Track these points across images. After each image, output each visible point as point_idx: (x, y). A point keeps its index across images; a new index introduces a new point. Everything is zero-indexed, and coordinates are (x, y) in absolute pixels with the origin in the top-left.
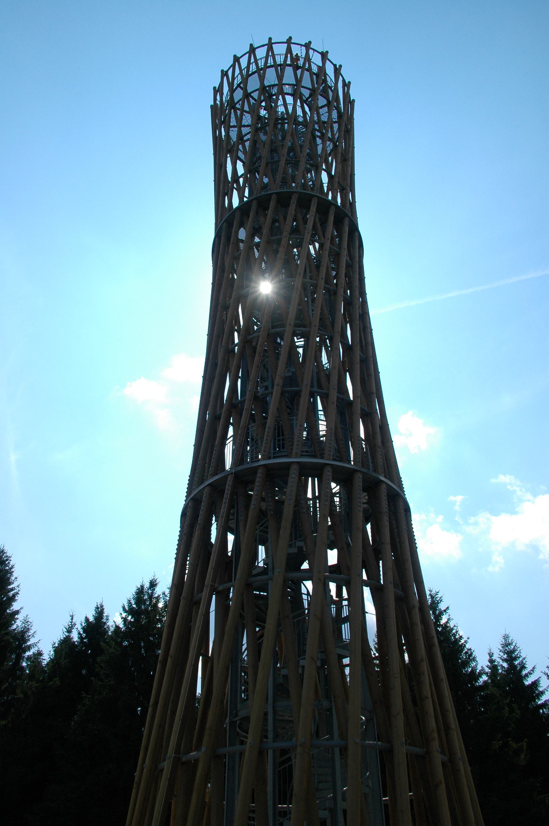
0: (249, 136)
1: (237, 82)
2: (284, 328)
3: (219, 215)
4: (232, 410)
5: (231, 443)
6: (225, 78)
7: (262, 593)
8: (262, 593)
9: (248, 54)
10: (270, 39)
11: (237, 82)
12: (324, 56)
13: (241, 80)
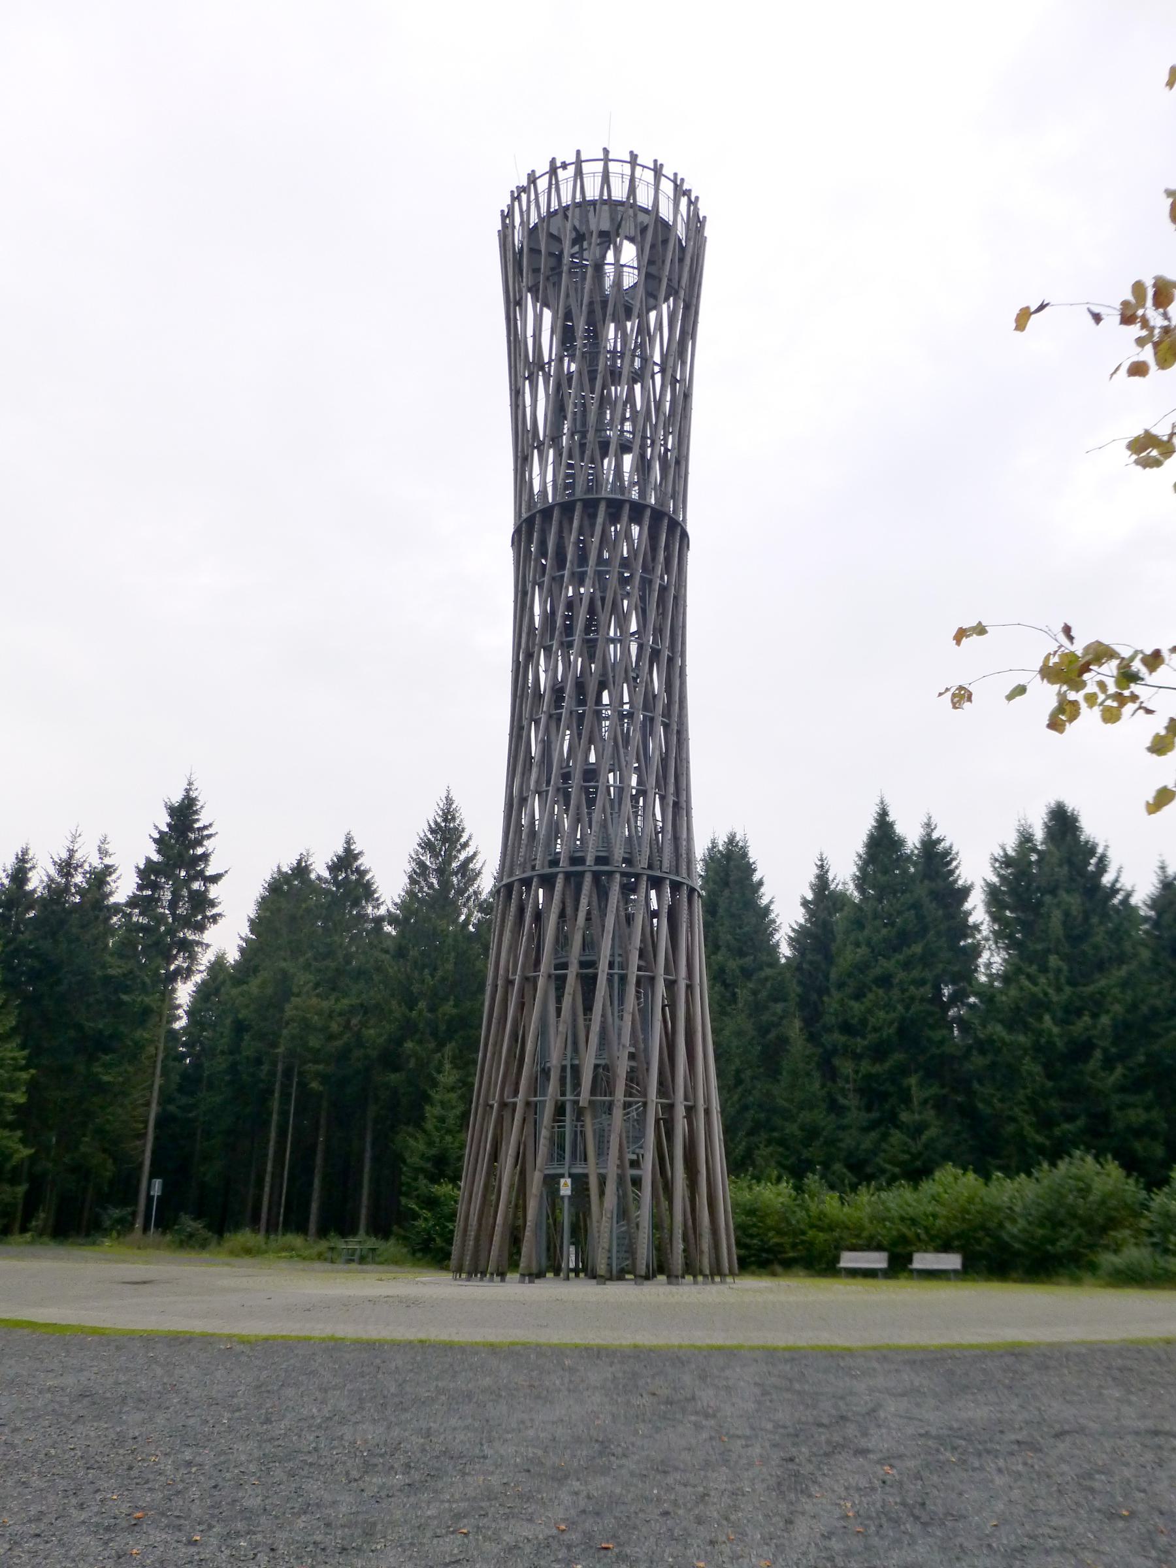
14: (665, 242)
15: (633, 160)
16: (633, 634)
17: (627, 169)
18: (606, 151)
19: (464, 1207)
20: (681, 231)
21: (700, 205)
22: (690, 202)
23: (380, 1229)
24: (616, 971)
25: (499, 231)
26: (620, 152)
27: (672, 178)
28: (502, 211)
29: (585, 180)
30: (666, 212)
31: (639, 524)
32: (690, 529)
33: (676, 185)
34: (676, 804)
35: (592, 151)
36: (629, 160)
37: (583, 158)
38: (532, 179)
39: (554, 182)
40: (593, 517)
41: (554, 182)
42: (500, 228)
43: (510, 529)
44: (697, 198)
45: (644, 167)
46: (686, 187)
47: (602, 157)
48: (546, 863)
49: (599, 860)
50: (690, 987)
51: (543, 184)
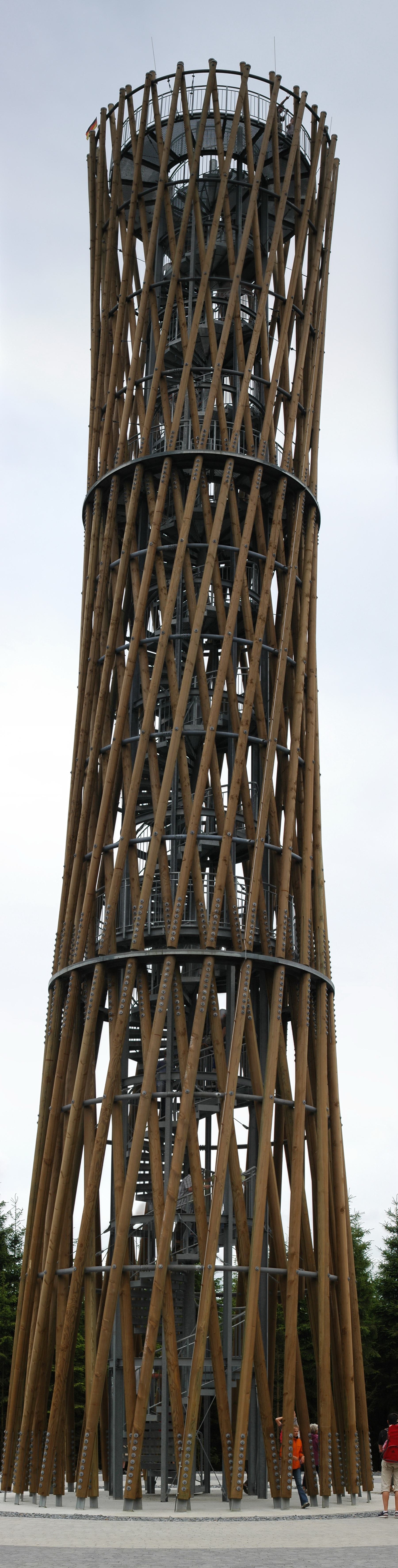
0: (152, 102)
1: (125, 142)
2: (188, 634)
3: (81, 740)
4: (113, 564)
5: (149, 122)
6: (108, 122)
7: (142, 1183)
8: (142, 1183)
9: (143, 89)
10: (180, 65)
11: (125, 142)
12: (274, 81)
13: (130, 139)
14: (284, 156)
16: (116, 846)
17: (237, 80)
18: (213, 63)
19: (22, 1323)
20: (305, 146)
21: (327, 123)
22: (315, 119)
25: (88, 156)
31: (218, 481)
32: (322, 500)
34: (299, 585)
35: (196, 61)
38: (127, 94)
39: (151, 98)
40: (185, 481)
41: (151, 98)
43: (82, 493)
44: (324, 114)
46: (310, 102)
47: (208, 68)
48: (114, 947)
49: (184, 940)
51: (138, 99)
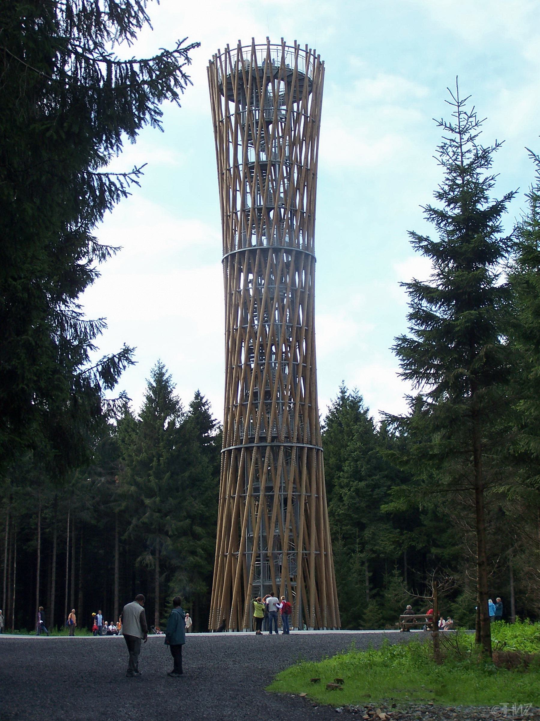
15: (284, 45)
23: (15, 629)
24: (282, 493)
25: (207, 67)
26: (275, 40)
27: (305, 50)
28: (210, 61)
29: (257, 53)
30: (302, 68)
33: (307, 53)
36: (281, 44)
37: (256, 44)
42: (208, 65)
45: (289, 47)
47: (266, 43)
49: (273, 439)
50: (318, 498)
